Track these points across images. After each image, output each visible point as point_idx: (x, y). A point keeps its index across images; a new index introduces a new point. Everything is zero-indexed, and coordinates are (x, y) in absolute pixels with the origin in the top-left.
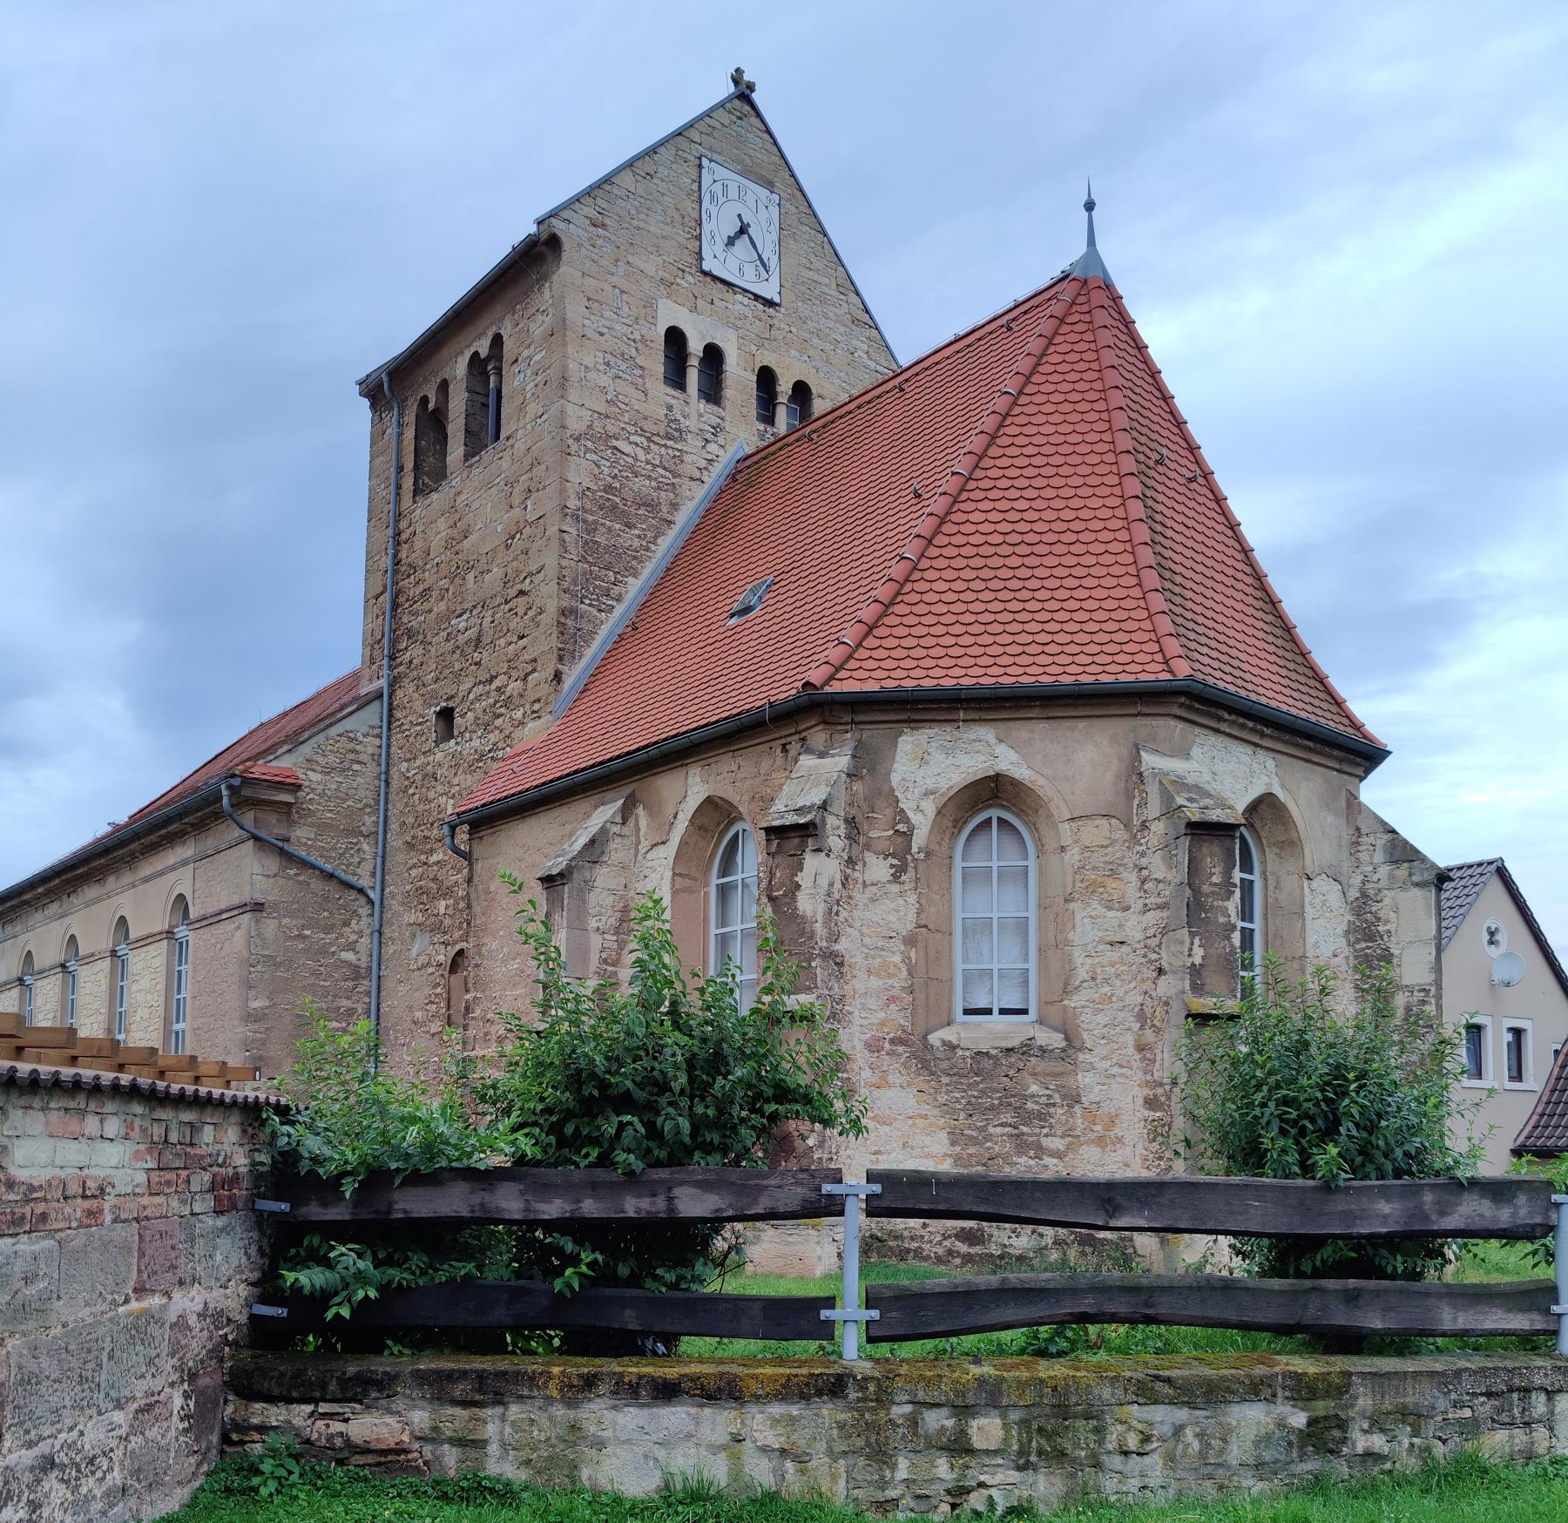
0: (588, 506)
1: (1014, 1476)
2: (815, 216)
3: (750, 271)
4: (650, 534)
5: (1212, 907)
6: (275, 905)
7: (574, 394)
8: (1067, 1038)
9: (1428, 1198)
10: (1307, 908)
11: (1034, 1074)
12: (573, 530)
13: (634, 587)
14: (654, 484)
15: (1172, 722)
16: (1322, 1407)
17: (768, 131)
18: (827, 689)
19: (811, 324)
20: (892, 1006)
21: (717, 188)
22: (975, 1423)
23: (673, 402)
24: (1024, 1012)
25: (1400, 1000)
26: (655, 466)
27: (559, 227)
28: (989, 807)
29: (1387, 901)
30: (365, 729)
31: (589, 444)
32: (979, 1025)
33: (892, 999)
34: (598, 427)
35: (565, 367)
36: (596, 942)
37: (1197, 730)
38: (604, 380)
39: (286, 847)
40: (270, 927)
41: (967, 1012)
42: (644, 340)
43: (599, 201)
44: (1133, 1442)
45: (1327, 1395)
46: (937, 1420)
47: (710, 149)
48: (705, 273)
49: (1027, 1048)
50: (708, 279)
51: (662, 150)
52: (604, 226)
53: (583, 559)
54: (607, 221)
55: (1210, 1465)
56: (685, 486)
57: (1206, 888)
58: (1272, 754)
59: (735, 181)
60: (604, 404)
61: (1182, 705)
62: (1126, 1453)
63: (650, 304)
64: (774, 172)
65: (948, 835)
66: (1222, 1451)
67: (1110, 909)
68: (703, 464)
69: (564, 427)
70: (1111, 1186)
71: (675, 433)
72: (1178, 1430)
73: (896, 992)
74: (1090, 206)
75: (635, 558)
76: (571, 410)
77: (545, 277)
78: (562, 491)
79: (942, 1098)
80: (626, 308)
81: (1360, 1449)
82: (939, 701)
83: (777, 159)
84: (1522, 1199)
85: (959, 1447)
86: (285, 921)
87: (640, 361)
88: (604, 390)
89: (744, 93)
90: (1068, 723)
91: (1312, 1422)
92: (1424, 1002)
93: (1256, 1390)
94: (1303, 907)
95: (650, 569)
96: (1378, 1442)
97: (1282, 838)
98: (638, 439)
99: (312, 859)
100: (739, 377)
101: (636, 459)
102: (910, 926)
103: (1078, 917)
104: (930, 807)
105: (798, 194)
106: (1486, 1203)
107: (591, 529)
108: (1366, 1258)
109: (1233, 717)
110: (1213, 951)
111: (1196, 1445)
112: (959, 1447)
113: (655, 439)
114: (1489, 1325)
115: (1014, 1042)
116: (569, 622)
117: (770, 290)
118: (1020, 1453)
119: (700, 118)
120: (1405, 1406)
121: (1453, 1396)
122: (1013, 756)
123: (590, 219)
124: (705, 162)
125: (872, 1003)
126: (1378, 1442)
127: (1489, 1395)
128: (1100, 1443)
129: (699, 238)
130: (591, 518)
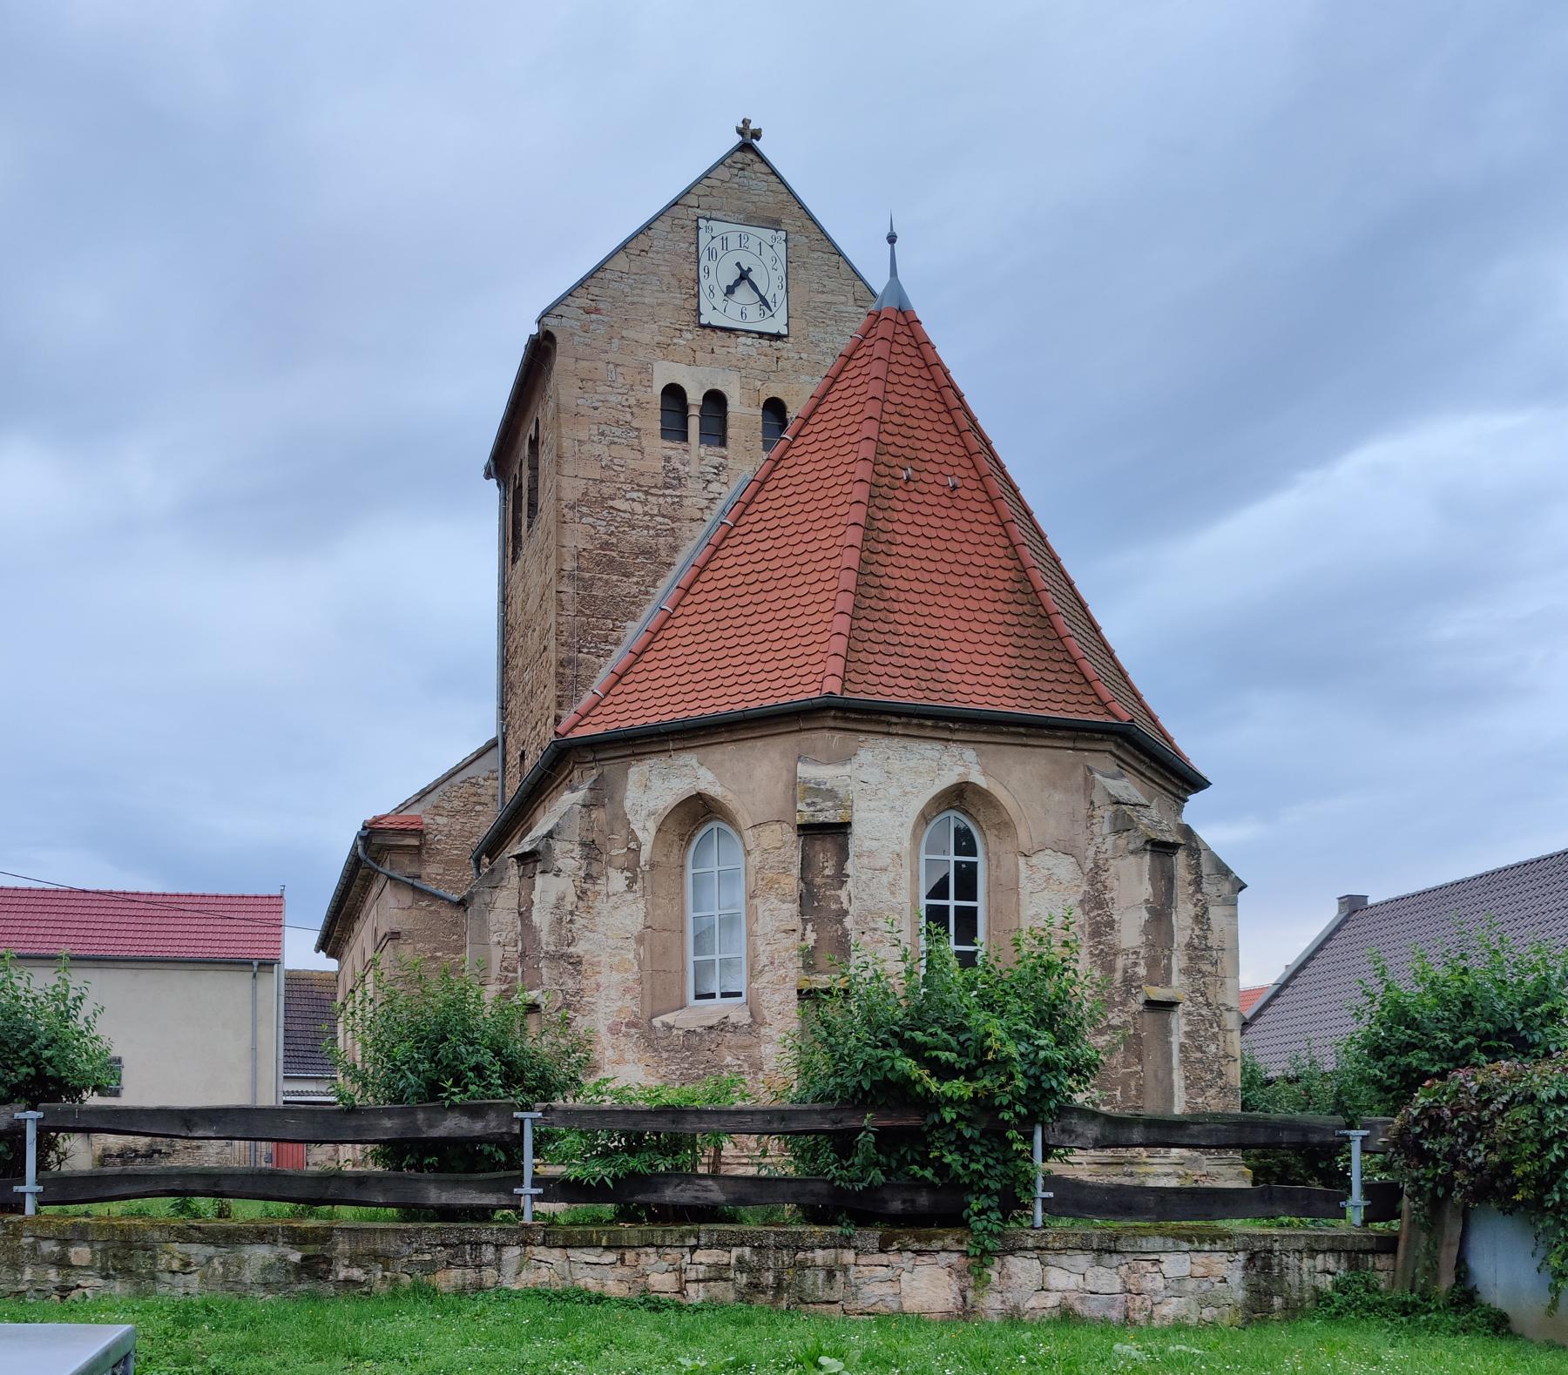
0: (585, 564)
1: (100, 1282)
2: (829, 239)
3: (754, 312)
4: (648, 579)
5: (825, 896)
6: (410, 934)
7: (568, 469)
8: (752, 1015)
9: (421, 1116)
10: (1023, 882)
11: (729, 1047)
12: (570, 590)
13: (632, 633)
14: (652, 532)
15: (827, 734)
16: (311, 1249)
17: (774, 173)
18: (570, 736)
20: (628, 996)
21: (717, 244)
22: (73, 1250)
23: (671, 453)
24: (739, 994)
25: (1120, 963)
26: (652, 516)
27: (552, 323)
28: (710, 820)
29: (1112, 870)
30: (486, 774)
31: (584, 509)
32: (703, 1007)
33: (627, 990)
34: (593, 492)
35: (559, 446)
36: (497, 954)
37: (862, 737)
38: (599, 449)
39: (417, 883)
40: (406, 951)
41: (698, 997)
42: (639, 404)
43: (592, 290)
44: (176, 1265)
45: (315, 1241)
46: (49, 1247)
47: (709, 209)
48: (704, 327)
49: (723, 1026)
50: (708, 331)
51: (657, 224)
52: (597, 311)
53: (580, 613)
54: (601, 306)
55: (231, 1282)
56: (685, 529)
57: (818, 881)
59: (731, 231)
60: (599, 471)
61: (835, 718)
62: (174, 1272)
63: (645, 370)
64: (784, 212)
65: (675, 850)
66: (238, 1274)
67: (784, 902)
68: (705, 503)
69: (559, 499)
70: (192, 1112)
71: (674, 480)
72: (210, 1259)
73: (630, 984)
74: (892, 239)
75: (633, 603)
76: (565, 482)
77: (551, 369)
78: (559, 556)
79: (662, 1071)
80: (620, 380)
81: (341, 1276)
82: (651, 736)
83: (785, 197)
84: (492, 1116)
85: (62, 1263)
86: (419, 946)
87: (634, 424)
88: (599, 458)
89: (748, 142)
90: (749, 744)
91: (304, 1259)
92: (1135, 964)
93: (262, 1235)
94: (1017, 882)
95: (647, 615)
96: (357, 1273)
97: (997, 821)
98: (635, 495)
99: (441, 892)
100: (743, 413)
101: (633, 513)
102: (640, 927)
103: (760, 911)
104: (652, 827)
106: (465, 1119)
107: (588, 585)
108: (460, 1158)
109: (904, 720)
110: (826, 935)
111: (221, 1269)
112: (62, 1263)
113: (653, 491)
114: (466, 1201)
115: (714, 1021)
116: (568, 671)
117: (777, 325)
118: (102, 1269)
119: (698, 182)
120: (375, 1251)
121: (415, 1245)
122: (710, 776)
124: (702, 223)
125: (614, 994)
126: (357, 1273)
127: (445, 1246)
128: (154, 1264)
129: (697, 295)
130: (587, 575)
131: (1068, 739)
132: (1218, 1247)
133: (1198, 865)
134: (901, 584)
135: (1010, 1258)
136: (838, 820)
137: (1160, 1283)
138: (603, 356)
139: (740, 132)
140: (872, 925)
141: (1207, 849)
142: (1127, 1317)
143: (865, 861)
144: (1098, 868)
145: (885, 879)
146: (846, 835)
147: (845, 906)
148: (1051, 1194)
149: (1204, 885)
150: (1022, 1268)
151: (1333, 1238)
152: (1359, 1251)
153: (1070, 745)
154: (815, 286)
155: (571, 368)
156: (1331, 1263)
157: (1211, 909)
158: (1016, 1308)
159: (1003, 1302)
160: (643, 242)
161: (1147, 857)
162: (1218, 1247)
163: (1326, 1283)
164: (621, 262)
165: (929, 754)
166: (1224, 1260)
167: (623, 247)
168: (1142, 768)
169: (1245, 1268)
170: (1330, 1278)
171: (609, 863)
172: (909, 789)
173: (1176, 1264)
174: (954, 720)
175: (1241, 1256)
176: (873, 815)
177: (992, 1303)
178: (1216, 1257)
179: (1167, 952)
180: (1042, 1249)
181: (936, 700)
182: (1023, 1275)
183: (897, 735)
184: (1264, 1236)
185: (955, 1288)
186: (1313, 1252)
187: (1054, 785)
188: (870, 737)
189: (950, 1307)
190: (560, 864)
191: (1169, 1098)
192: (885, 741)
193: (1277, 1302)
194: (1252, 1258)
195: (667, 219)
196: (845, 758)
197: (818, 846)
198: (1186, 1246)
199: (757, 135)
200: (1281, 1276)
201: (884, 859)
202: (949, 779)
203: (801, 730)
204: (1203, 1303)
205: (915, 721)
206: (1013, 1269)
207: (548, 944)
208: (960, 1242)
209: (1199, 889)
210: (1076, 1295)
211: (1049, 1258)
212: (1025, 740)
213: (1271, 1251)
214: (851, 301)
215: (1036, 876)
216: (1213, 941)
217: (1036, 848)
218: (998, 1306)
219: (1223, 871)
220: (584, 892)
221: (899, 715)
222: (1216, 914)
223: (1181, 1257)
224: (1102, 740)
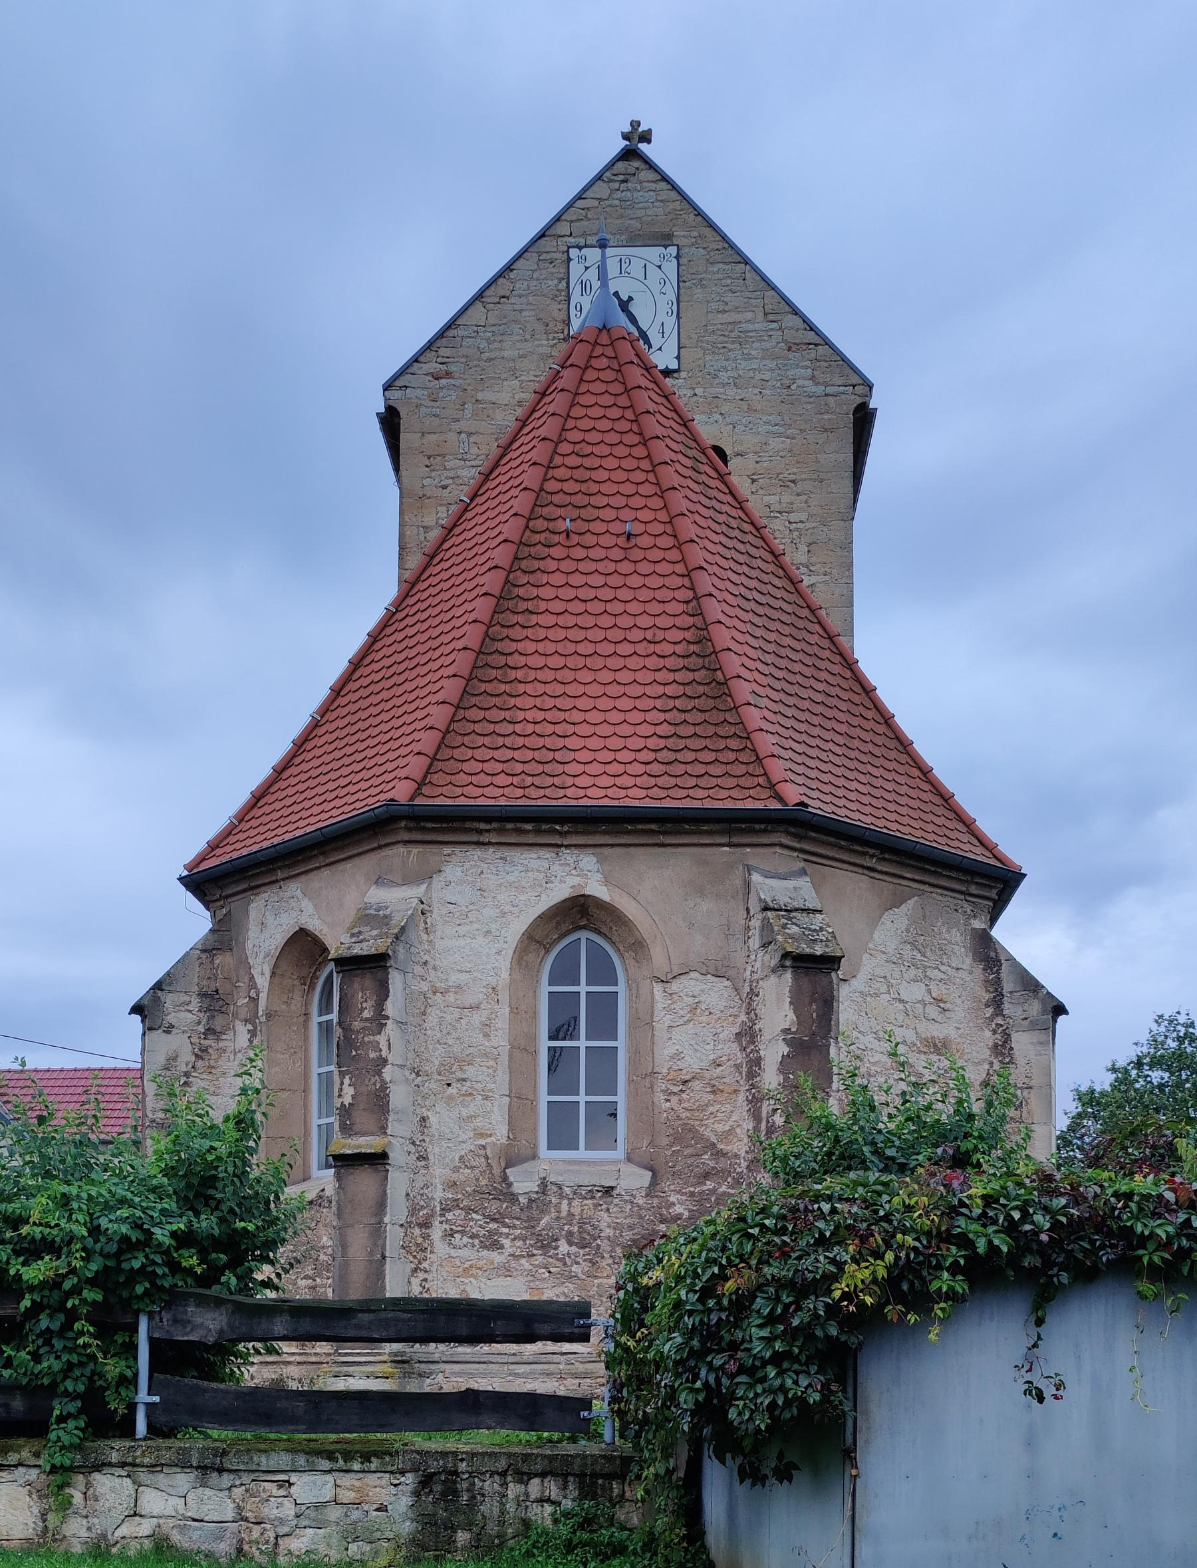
10: (659, 1014)
15: (401, 849)
19: (724, 376)
37: (447, 850)
43: (442, 352)
52: (448, 375)
54: (453, 368)
57: (357, 1025)
58: (591, 850)
61: (409, 829)
80: (474, 450)
89: (633, 150)
105: (707, 232)
109: (495, 825)
110: (363, 1089)
123: (432, 374)
124: (574, 253)
131: (721, 833)
132: (373, 1467)
133: (998, 980)
134: (538, 661)
135: (96, 1475)
136: (373, 951)
137: (289, 1510)
138: (456, 426)
139: (626, 137)
140: (459, 1075)
141: (1011, 959)
142: (240, 1550)
143: (451, 998)
144: (753, 993)
145: (477, 1018)
146: (386, 968)
147: (384, 1054)
148: (156, 1399)
149: (1006, 1006)
150: (111, 1488)
151: (551, 1458)
152: (595, 1475)
153: (725, 840)
154: (714, 305)
155: (417, 445)
156: (552, 1488)
157: (1015, 1037)
158: (104, 1536)
159: (89, 1529)
160: (504, 286)
161: (788, 975)
162: (373, 1467)
163: (542, 1515)
164: (477, 314)
165: (534, 864)
166: (384, 1482)
167: (479, 296)
168: (872, 863)
169: (416, 1493)
170: (549, 1509)
171: (235, 1015)
172: (508, 908)
173: (312, 1487)
174: (562, 820)
175: (410, 1479)
176: (462, 942)
177: (76, 1530)
178: (372, 1479)
179: (820, 1095)
180: (134, 1465)
181: (538, 799)
182: (111, 1497)
183: (489, 843)
184: (444, 1454)
185: (36, 1511)
186: (523, 1477)
187: (701, 893)
188: (457, 849)
189: (30, 1533)
190: (171, 1019)
191: (377, 1274)
192: (478, 853)
193: (462, 1537)
194: (426, 1482)
195: (532, 256)
196: (426, 875)
197: (357, 983)
198: (325, 1464)
199: (646, 137)
200: (472, 1504)
201: (476, 995)
202: (560, 892)
203: (380, 847)
204: (351, 1535)
205: (509, 826)
206: (101, 1490)
207: (154, 1111)
208: (37, 1455)
209: (999, 1012)
210: (172, 1522)
211: (143, 1477)
212: (662, 839)
213: (455, 1473)
214: (760, 316)
215: (678, 1006)
216: (1017, 1076)
217: (676, 972)
218: (84, 1533)
219: (1031, 985)
220: (205, 1050)
221: (488, 820)
222: (1022, 1042)
223: (319, 1478)
224: (765, 831)
